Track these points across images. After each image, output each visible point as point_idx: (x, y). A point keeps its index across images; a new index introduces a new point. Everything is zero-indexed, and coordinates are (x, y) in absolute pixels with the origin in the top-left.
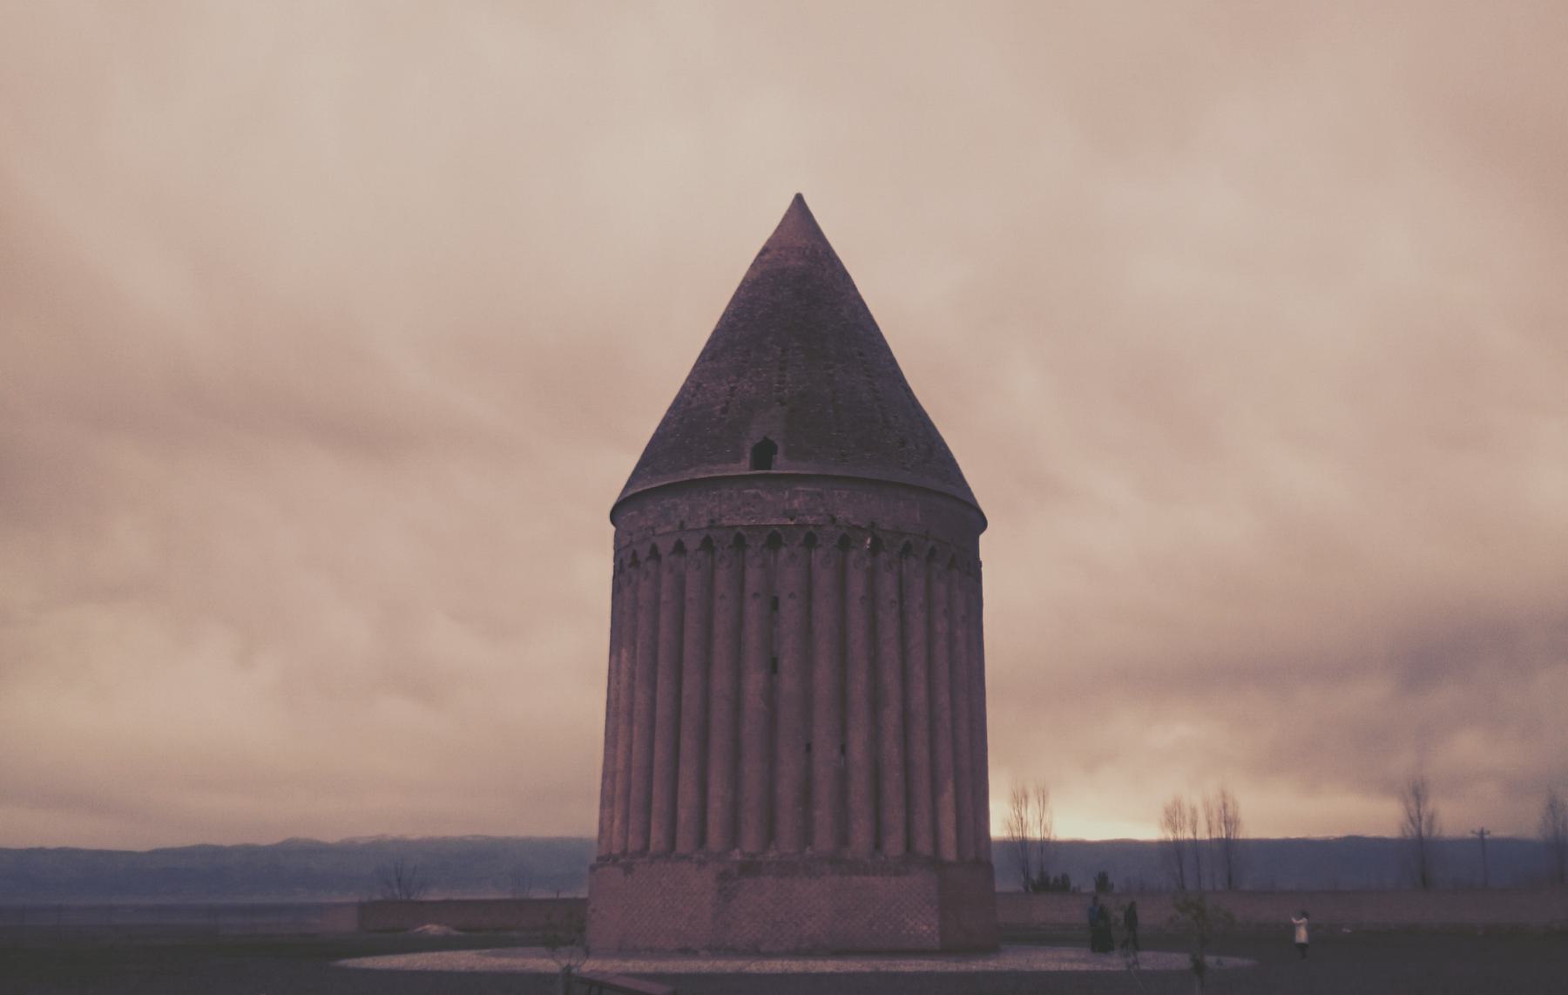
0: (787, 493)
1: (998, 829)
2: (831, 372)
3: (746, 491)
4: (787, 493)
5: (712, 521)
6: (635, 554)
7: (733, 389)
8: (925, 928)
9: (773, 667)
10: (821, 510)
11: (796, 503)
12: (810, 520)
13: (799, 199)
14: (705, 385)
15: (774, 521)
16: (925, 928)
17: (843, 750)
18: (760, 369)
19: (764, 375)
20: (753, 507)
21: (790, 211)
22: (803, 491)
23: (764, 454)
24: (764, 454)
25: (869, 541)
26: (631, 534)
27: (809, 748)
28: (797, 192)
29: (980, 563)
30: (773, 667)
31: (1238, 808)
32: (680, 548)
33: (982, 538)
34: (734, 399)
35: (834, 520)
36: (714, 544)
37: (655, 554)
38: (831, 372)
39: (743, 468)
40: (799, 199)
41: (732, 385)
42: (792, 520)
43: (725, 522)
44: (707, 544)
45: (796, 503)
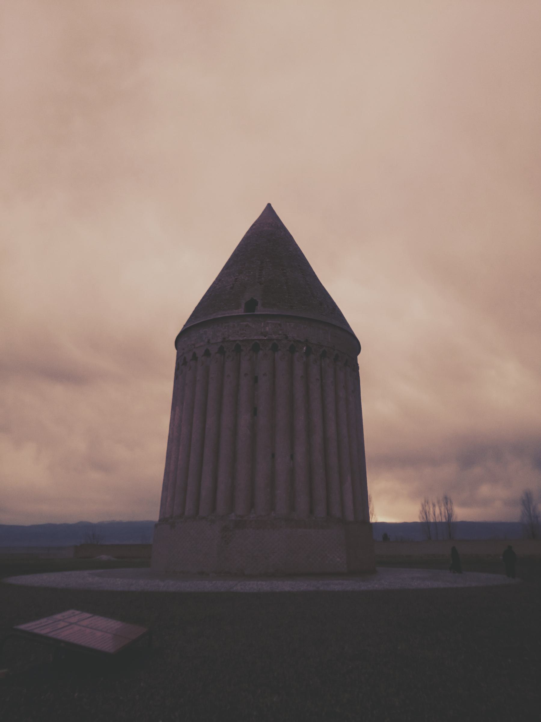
0: (263, 324)
1: (373, 520)
2: (285, 271)
3: (242, 323)
4: (263, 324)
5: (224, 339)
6: (185, 359)
7: (236, 279)
8: (338, 559)
9: (255, 412)
10: (280, 332)
11: (267, 329)
12: (274, 337)
13: (269, 205)
14: (223, 279)
15: (256, 338)
16: (338, 559)
17: (292, 457)
18: (250, 270)
19: (252, 273)
20: (245, 331)
21: (265, 210)
22: (271, 323)
23: (251, 305)
24: (251, 305)
25: (305, 349)
26: (184, 349)
27: (273, 456)
28: (270, 203)
29: (359, 367)
30: (255, 412)
31: (453, 510)
32: (207, 353)
33: (359, 357)
34: (237, 283)
35: (287, 337)
36: (225, 350)
37: (195, 357)
38: (285, 271)
39: (241, 312)
40: (269, 205)
41: (236, 277)
42: (265, 337)
43: (231, 338)
44: (221, 351)
45: (267, 329)
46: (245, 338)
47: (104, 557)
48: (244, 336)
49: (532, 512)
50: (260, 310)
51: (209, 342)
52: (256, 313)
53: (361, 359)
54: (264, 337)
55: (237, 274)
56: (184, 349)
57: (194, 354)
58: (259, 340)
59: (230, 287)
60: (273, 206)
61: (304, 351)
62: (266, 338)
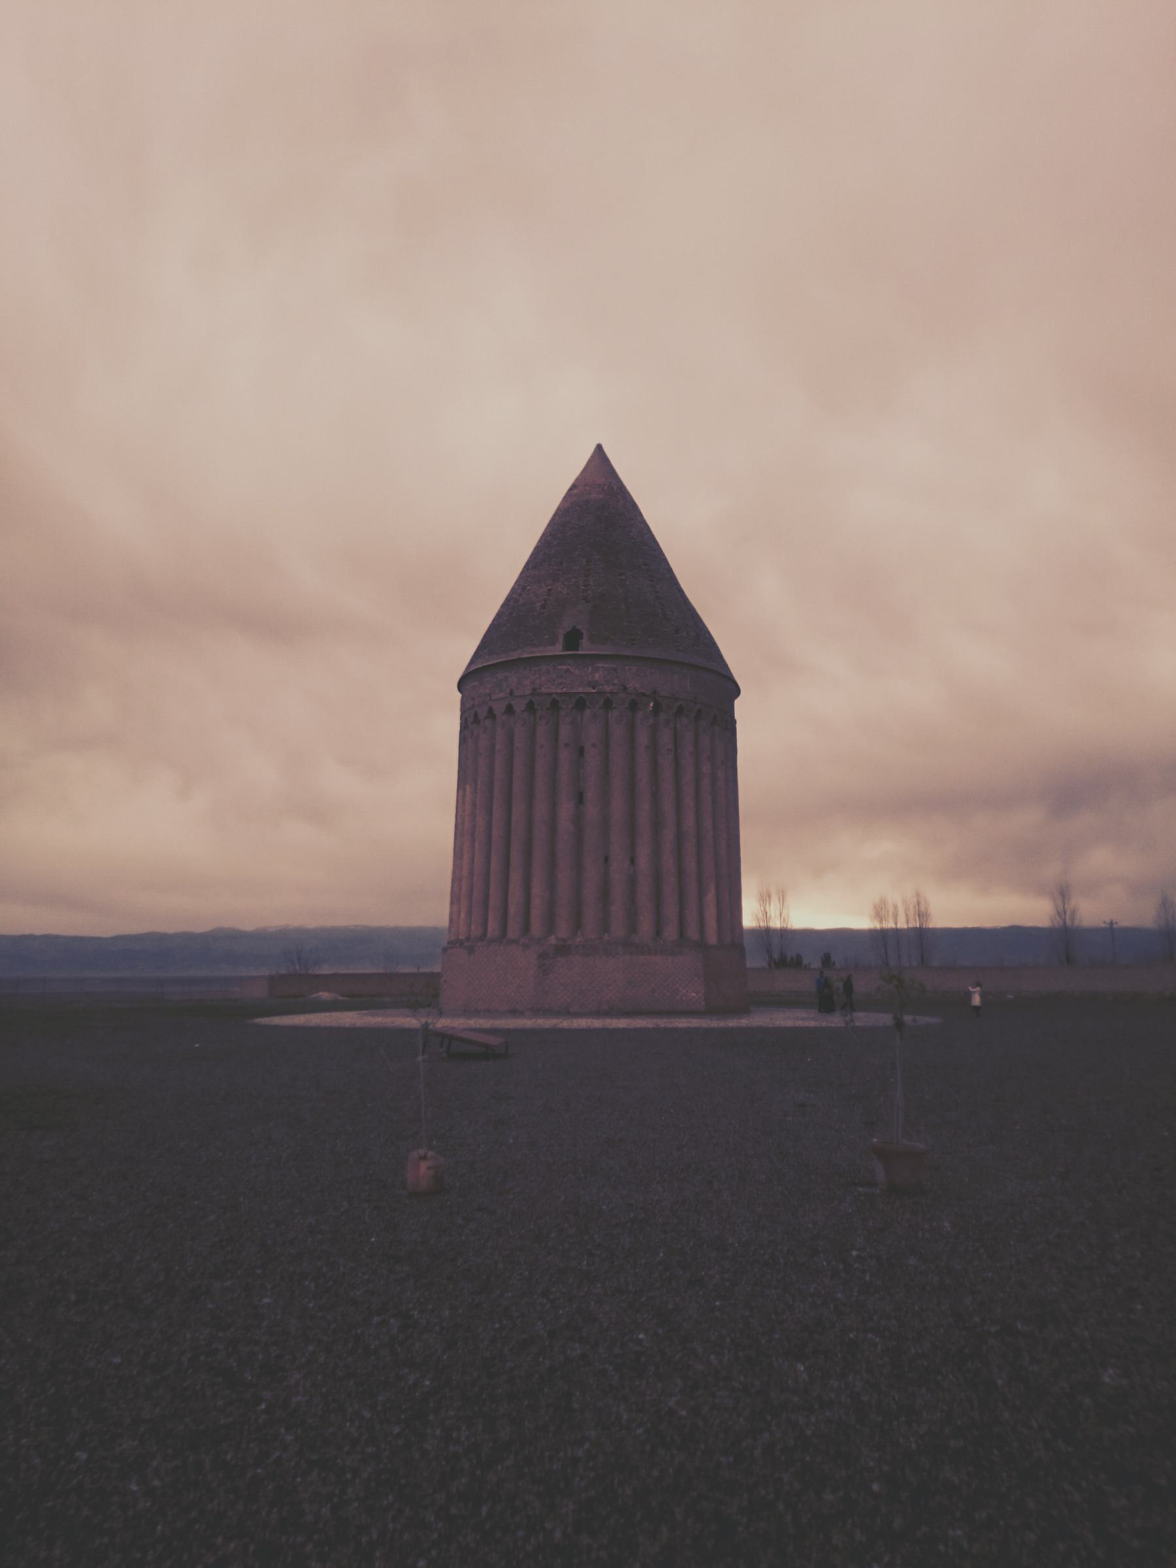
0: (590, 668)
2: (623, 577)
3: (559, 667)
4: (590, 668)
6: (476, 715)
7: (550, 590)
8: (694, 994)
9: (580, 798)
10: (616, 681)
12: (608, 688)
13: (599, 448)
14: (528, 588)
15: (581, 690)
16: (694, 994)
17: (633, 861)
23: (573, 639)
24: (573, 639)
27: (606, 859)
28: (601, 443)
30: (580, 798)
32: (510, 710)
35: (625, 689)
37: (491, 714)
38: (623, 577)
39: (558, 649)
40: (599, 448)
41: (549, 587)
42: (594, 688)
43: (543, 690)
44: (530, 707)
45: (597, 676)
46: (565, 689)
47: (325, 995)
48: (564, 687)
49: (1068, 920)
50: (586, 648)
51: (511, 693)
52: (580, 652)
53: (740, 707)
54: (591, 688)
55: (551, 582)
56: (473, 699)
57: (491, 710)
58: (585, 693)
59: (539, 604)
60: (606, 449)
61: (651, 709)
62: (594, 691)
